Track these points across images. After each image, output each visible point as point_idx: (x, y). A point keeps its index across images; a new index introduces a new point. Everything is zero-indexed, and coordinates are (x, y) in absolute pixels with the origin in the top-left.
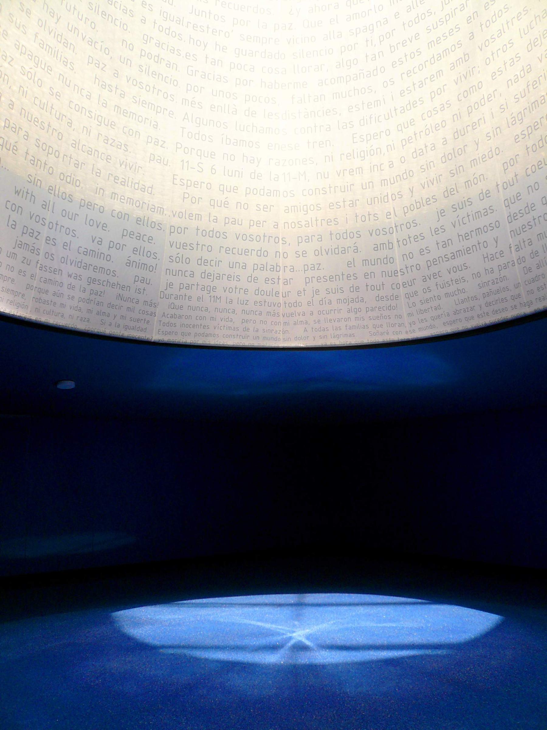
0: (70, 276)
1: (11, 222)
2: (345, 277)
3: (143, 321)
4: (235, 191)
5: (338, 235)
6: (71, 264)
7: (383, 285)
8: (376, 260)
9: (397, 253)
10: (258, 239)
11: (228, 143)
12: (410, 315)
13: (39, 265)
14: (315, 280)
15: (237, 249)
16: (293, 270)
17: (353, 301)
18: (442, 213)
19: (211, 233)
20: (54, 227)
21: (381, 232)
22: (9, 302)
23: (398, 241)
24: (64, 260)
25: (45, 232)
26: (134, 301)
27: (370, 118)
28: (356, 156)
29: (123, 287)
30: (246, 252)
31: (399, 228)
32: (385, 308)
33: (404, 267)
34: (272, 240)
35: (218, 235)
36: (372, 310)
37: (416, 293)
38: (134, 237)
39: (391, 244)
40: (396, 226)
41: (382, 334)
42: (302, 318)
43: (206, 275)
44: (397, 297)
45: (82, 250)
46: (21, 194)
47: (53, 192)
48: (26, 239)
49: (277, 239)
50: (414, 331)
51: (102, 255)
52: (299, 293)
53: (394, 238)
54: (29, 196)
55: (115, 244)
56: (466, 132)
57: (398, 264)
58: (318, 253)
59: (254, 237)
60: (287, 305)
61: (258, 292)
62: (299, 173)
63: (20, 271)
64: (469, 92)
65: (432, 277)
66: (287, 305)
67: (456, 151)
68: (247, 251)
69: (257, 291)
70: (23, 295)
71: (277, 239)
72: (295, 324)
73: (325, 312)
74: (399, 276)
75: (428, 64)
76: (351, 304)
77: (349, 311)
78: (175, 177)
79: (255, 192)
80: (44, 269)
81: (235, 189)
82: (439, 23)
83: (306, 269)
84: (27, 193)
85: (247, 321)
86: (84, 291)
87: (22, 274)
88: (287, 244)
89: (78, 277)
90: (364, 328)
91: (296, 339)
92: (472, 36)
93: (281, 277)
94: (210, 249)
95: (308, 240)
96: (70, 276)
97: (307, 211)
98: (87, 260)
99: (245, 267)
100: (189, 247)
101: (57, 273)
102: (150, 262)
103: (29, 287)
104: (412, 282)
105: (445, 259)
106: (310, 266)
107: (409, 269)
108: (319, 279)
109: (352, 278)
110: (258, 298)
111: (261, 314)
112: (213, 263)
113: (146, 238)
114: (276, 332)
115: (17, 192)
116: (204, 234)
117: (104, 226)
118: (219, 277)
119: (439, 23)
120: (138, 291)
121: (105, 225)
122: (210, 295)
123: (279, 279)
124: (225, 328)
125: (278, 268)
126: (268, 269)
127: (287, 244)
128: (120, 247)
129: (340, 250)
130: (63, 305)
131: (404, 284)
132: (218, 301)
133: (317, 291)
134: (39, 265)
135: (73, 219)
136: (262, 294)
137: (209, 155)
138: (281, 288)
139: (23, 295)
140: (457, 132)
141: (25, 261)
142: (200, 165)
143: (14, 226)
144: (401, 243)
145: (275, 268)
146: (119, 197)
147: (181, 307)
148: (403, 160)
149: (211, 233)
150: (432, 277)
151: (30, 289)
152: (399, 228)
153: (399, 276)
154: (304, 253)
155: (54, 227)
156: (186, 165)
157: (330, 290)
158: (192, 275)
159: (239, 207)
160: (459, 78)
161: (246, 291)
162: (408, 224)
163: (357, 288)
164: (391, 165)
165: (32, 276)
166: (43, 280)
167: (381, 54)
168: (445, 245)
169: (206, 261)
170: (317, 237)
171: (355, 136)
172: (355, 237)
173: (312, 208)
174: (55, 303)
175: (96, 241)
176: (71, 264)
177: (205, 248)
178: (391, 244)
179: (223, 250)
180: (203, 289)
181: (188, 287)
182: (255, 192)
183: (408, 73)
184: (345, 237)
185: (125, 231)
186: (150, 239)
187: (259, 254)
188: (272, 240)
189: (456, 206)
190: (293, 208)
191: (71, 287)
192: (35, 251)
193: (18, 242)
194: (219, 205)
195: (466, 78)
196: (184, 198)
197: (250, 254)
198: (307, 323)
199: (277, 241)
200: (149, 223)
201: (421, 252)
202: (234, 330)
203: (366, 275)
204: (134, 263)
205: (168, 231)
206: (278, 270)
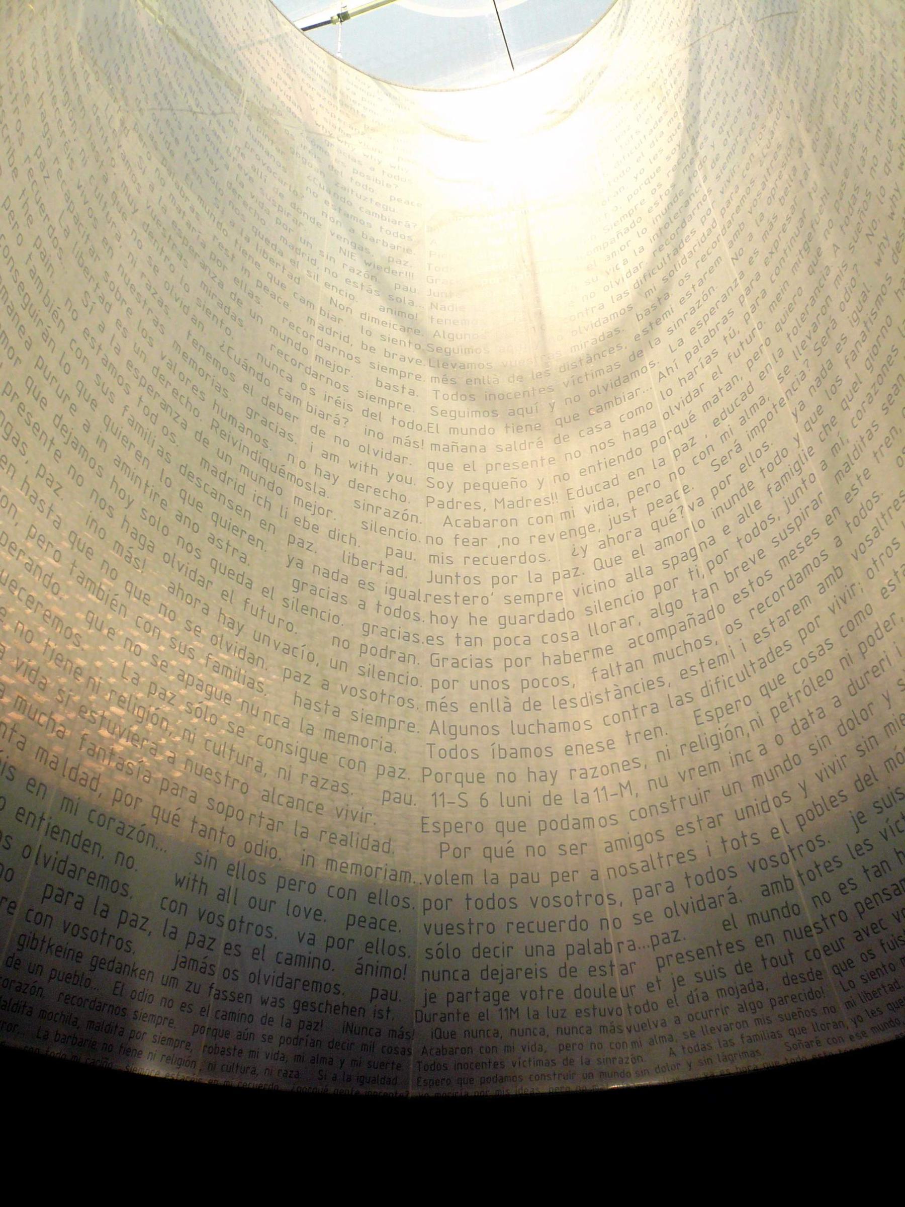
0: (264, 1002)
1: (169, 929)
2: (723, 948)
3: (389, 1066)
4: (521, 829)
5: (699, 878)
6: (686, 912)
7: (790, 954)
8: (770, 913)
9: (801, 895)
10: (568, 902)
11: (503, 755)
12: (849, 1004)
13: (214, 992)
14: (673, 960)
15: (535, 923)
16: (633, 947)
17: (744, 989)
18: (860, 818)
19: (491, 902)
20: (238, 927)
21: (727, 873)
22: (165, 1059)
23: (800, 875)
24: (255, 977)
25: (224, 936)
26: (584, 1030)
27: (717, 683)
28: (705, 745)
29: (352, 1011)
30: (551, 926)
31: (796, 852)
32: (802, 997)
33: (820, 919)
34: (591, 900)
35: (502, 904)
36: (782, 1001)
37: (849, 963)
38: (367, 924)
39: (789, 882)
40: (791, 850)
41: (808, 1045)
42: (661, 1031)
43: (489, 974)
44: (819, 974)
45: (282, 958)
46: (184, 885)
47: (234, 873)
48: (196, 953)
49: (599, 898)
50: (864, 1034)
51: (316, 961)
52: (649, 986)
53: (792, 869)
54: (197, 885)
55: (336, 940)
56: (865, 682)
57: (809, 916)
58: (670, 912)
59: (562, 900)
60: (633, 1010)
61: (580, 992)
62: (621, 785)
63: (183, 1006)
64: (854, 621)
65: (870, 931)
66: (633, 1010)
67: (858, 715)
68: (552, 924)
69: (578, 992)
70: (189, 1044)
71: (599, 898)
72: (652, 1042)
73: (699, 1016)
74: (815, 935)
75: (786, 590)
76: (743, 996)
77: (741, 1009)
78: (425, 821)
79: (554, 827)
80: (221, 996)
81: (521, 826)
82: (788, 531)
83: (655, 942)
84: (195, 880)
85: (567, 1047)
86: (289, 1025)
87: (186, 1009)
88: (618, 903)
89: (278, 1002)
90: (773, 1036)
91: (659, 1069)
92: (839, 543)
93: (615, 962)
94: (491, 929)
95: (651, 892)
96: (264, 1002)
97: (642, 845)
98: (293, 971)
99: (552, 952)
100: (456, 930)
101: (243, 1000)
102: (396, 962)
103: (198, 1029)
104: (839, 945)
105: (884, 897)
106: (661, 937)
107: (829, 921)
108: (679, 957)
109: (736, 948)
110: (582, 1004)
111: (589, 1031)
112: (499, 952)
113: (385, 924)
114: (621, 1062)
115: (179, 882)
116: (479, 906)
117: (318, 914)
118: (511, 975)
119: (788, 531)
120: (378, 1014)
121: (318, 912)
122: (499, 1007)
123: (612, 966)
124: (532, 1063)
125: (608, 946)
126: (592, 950)
127: (618, 903)
128: (344, 944)
129: (707, 902)
130: (253, 1054)
131: (826, 949)
132: (514, 1016)
133: (680, 980)
134: (214, 992)
135: (268, 909)
136: (587, 995)
137: (475, 779)
138: (618, 981)
139: (189, 1044)
140: (852, 684)
141: (191, 988)
142: (462, 796)
143: (173, 935)
144: (804, 877)
145: (603, 948)
146: (339, 866)
147: (453, 1035)
148: (779, 740)
149: (491, 902)
150: (870, 931)
151: (199, 1033)
152: (796, 852)
153: (815, 935)
154: (648, 916)
155: (238, 927)
156: (439, 800)
157: (703, 976)
158: (467, 976)
159: (531, 853)
160: (835, 604)
161: (559, 994)
162: (810, 844)
163: (748, 967)
164: (764, 751)
165: (203, 1010)
166: (220, 1014)
167: (714, 587)
168: (878, 873)
169: (486, 952)
170: (665, 886)
171: (698, 713)
172: (727, 877)
173: (649, 838)
174: (241, 1052)
175: (305, 940)
176: (686, 912)
177: (482, 929)
178: (789, 882)
179: (513, 928)
180: (486, 999)
181: (462, 998)
182: (554, 827)
183: (760, 608)
184: (711, 879)
185: (351, 918)
186: (393, 924)
187: (573, 927)
188: (591, 900)
189: (881, 804)
190: (618, 842)
191: (268, 1020)
192: (207, 969)
193: (181, 959)
194: (499, 854)
195: (845, 602)
196: (442, 851)
197: (557, 928)
198: (671, 1039)
199: (600, 901)
200: (389, 900)
201: (842, 888)
202: (547, 1064)
203: (758, 941)
204: (369, 968)
205: (420, 909)
206: (608, 950)
